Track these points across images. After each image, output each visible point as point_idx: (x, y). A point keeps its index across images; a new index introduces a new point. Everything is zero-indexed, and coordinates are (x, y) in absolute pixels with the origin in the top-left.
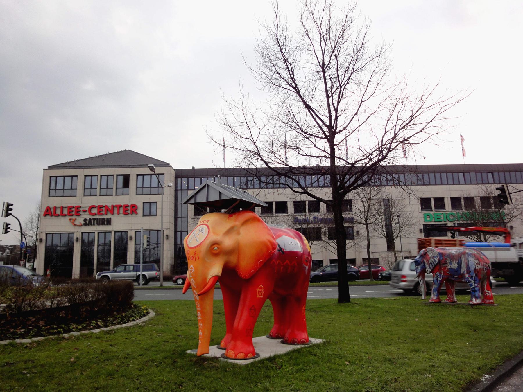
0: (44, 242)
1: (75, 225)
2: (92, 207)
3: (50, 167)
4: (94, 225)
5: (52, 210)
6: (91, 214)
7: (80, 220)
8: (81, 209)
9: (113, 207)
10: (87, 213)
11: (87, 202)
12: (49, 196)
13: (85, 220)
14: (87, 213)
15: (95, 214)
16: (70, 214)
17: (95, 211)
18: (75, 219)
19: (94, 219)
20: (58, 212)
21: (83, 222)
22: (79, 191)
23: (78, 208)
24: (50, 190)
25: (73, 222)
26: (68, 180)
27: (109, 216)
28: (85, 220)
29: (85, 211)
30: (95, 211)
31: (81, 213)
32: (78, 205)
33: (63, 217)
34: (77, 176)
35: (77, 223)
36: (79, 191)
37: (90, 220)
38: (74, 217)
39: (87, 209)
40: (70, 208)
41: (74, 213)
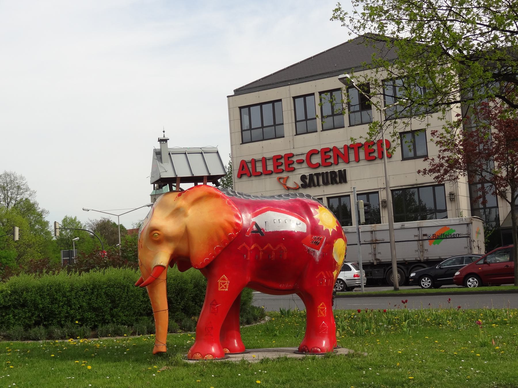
1: (288, 188)
3: (239, 92)
4: (319, 185)
6: (311, 166)
7: (294, 179)
8: (295, 159)
9: (346, 148)
10: (305, 165)
11: (303, 144)
12: (297, 134)
16: (277, 170)
17: (316, 159)
18: (288, 177)
21: (300, 183)
22: (289, 128)
25: (283, 182)
26: (268, 109)
28: (303, 178)
29: (300, 162)
31: (295, 166)
32: (288, 152)
33: (268, 177)
34: (280, 100)
35: (290, 184)
36: (289, 128)
37: (311, 176)
38: (284, 175)
40: (277, 159)
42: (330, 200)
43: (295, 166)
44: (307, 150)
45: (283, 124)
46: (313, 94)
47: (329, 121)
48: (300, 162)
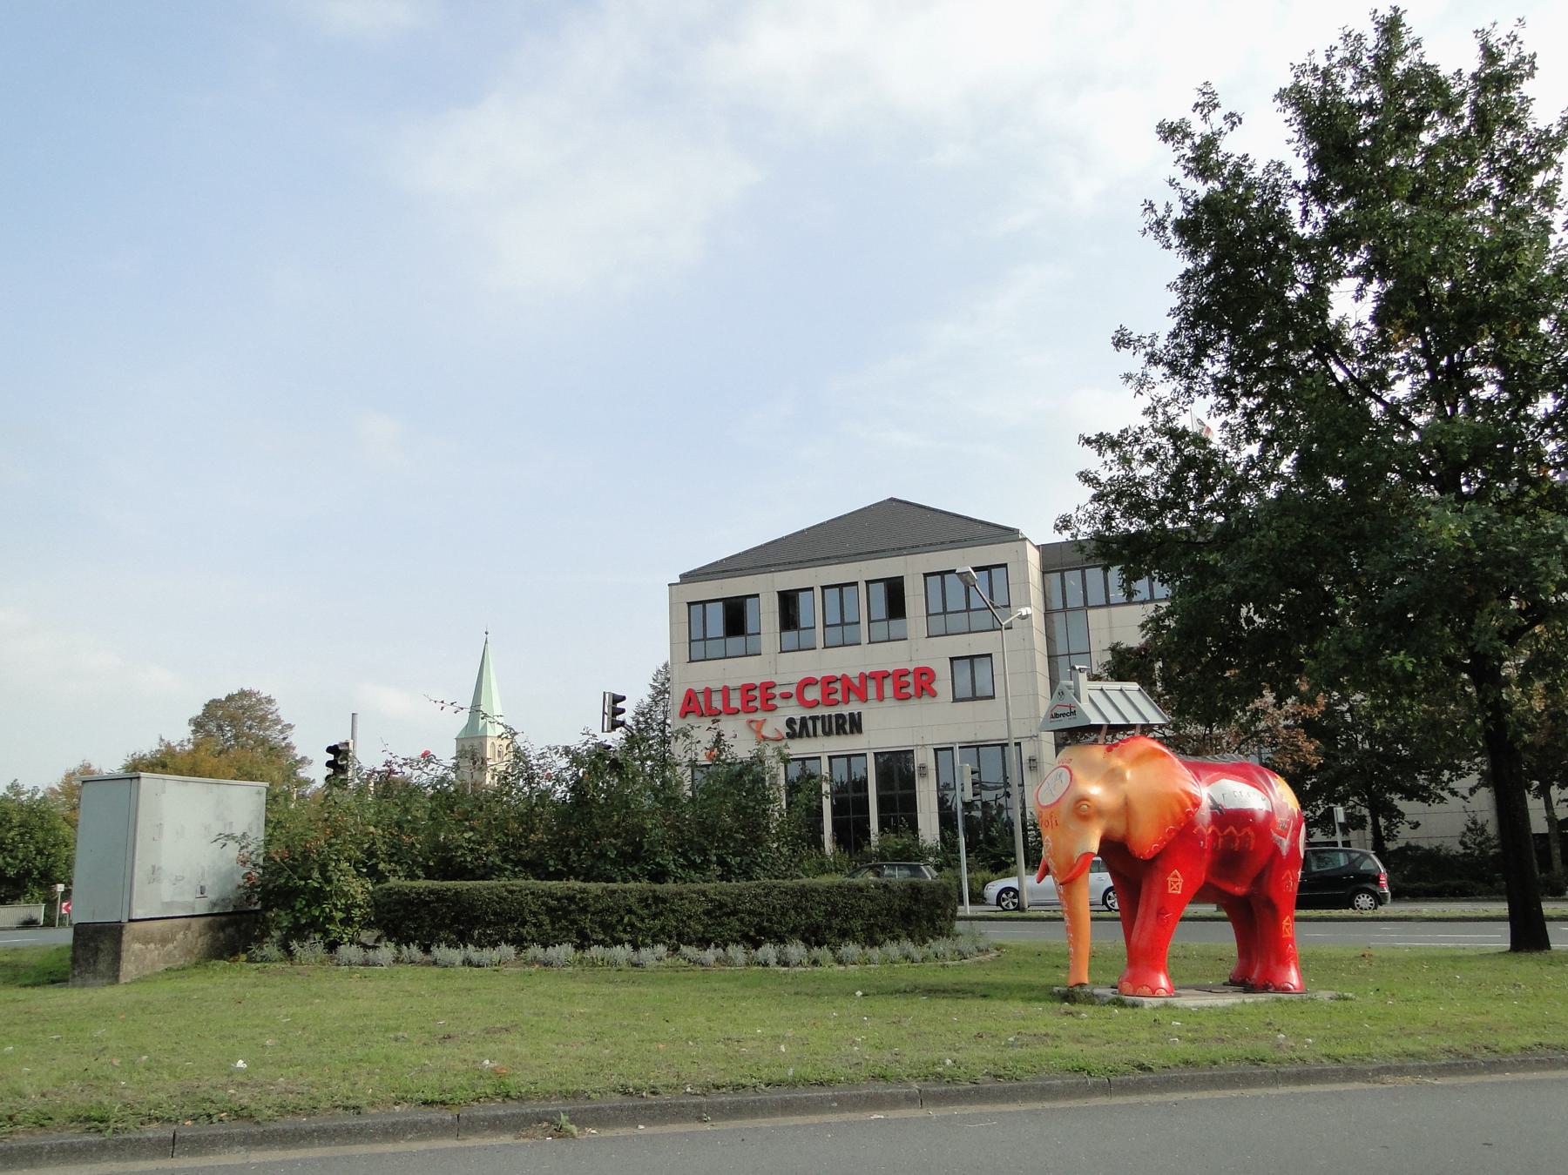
0: (932, 774)
7: (775, 724)
8: (777, 691)
10: (794, 701)
17: (813, 694)
21: (785, 730)
24: (691, 641)
28: (790, 722)
29: (786, 696)
34: (1005, 565)
38: (758, 716)
40: (747, 689)
46: (856, 584)
47: (835, 634)
48: (786, 696)
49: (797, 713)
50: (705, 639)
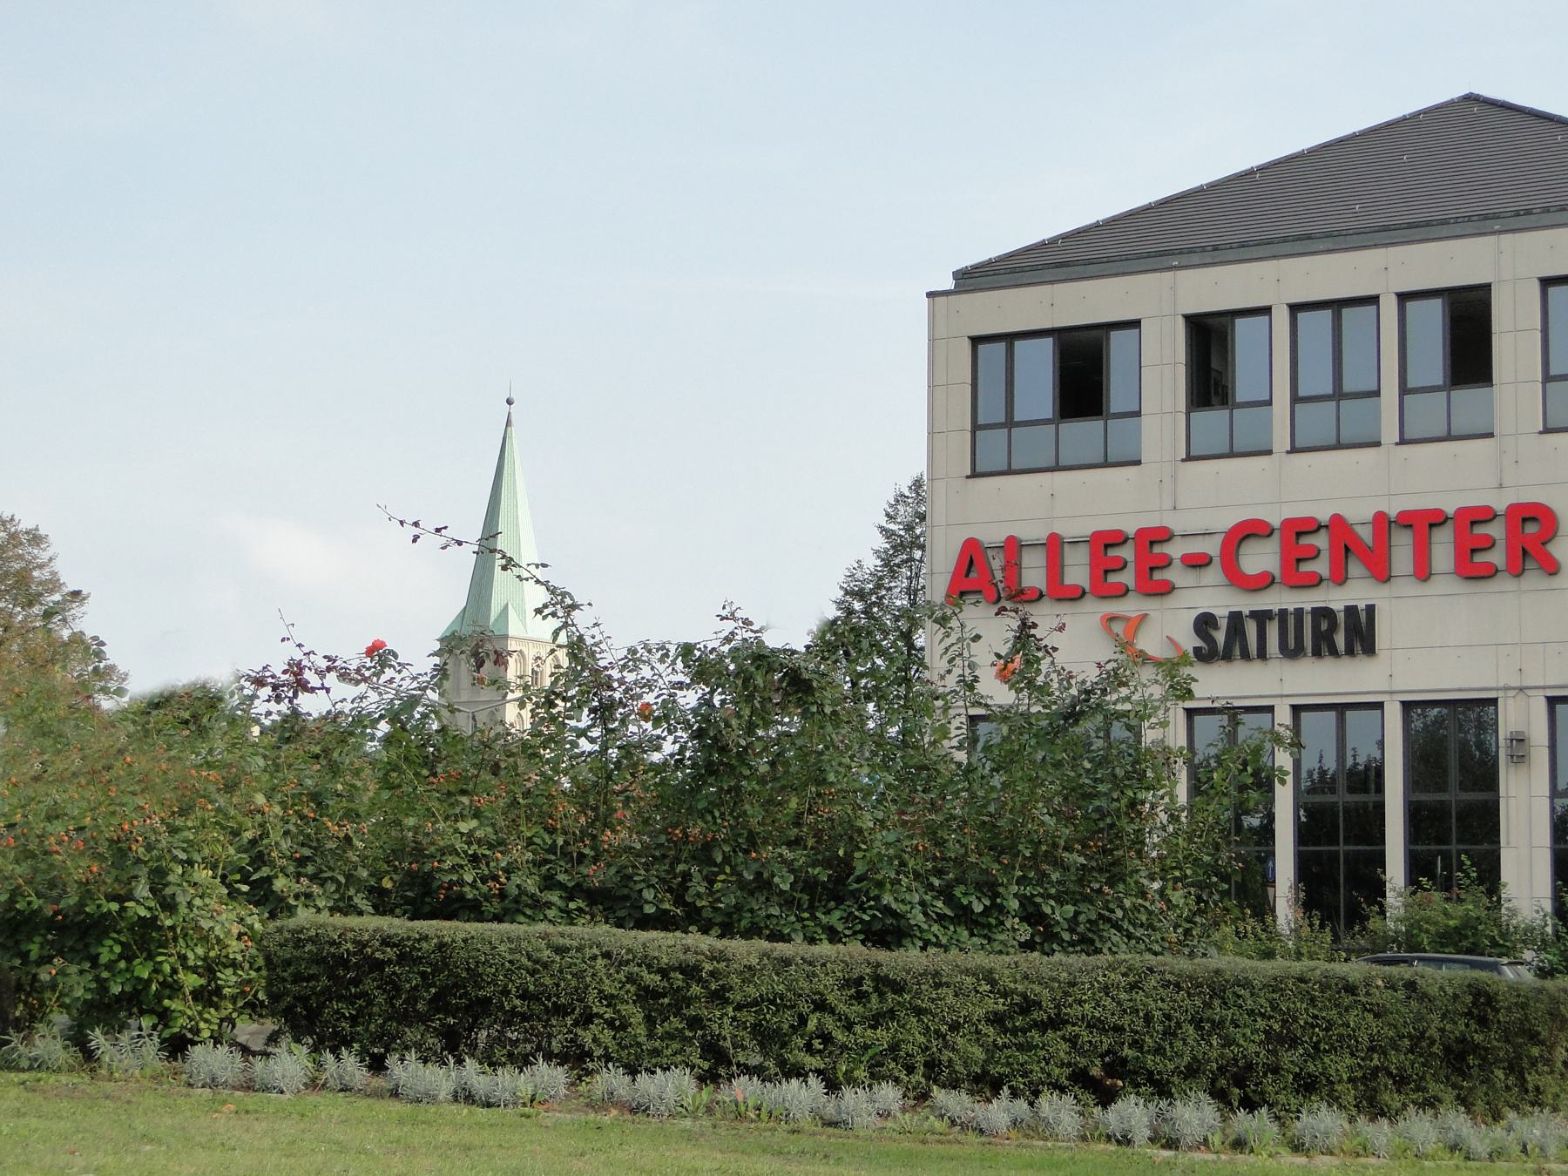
2: (1250, 531)
4: (1262, 655)
5: (997, 563)
6: (1237, 579)
8: (1175, 550)
12: (975, 474)
13: (1205, 623)
14: (1214, 574)
15: (1263, 582)
17: (1260, 558)
19: (1261, 617)
20: (1034, 574)
21: (1190, 641)
23: (1155, 537)
24: (976, 427)
27: (1357, 592)
28: (1205, 623)
29: (1197, 562)
30: (1260, 558)
31: (1175, 575)
34: (1135, 324)
37: (1236, 619)
38: (1130, 607)
39: (1212, 547)
40: (1105, 542)
41: (1127, 578)
42: (1304, 715)
43: (1175, 575)
44: (1228, 520)
45: (1138, 414)
48: (1197, 562)
49: (1222, 601)
50: (1010, 423)
